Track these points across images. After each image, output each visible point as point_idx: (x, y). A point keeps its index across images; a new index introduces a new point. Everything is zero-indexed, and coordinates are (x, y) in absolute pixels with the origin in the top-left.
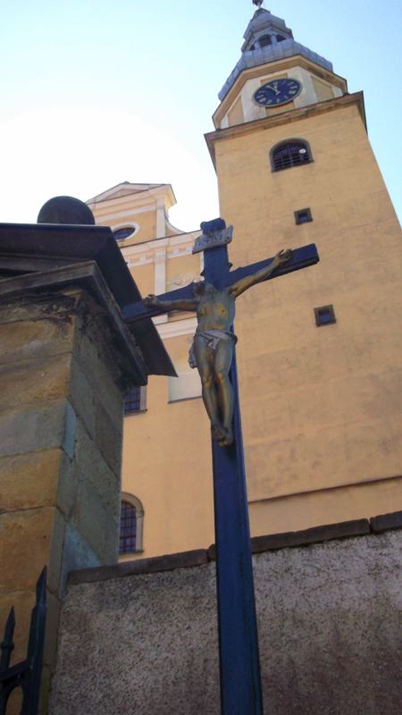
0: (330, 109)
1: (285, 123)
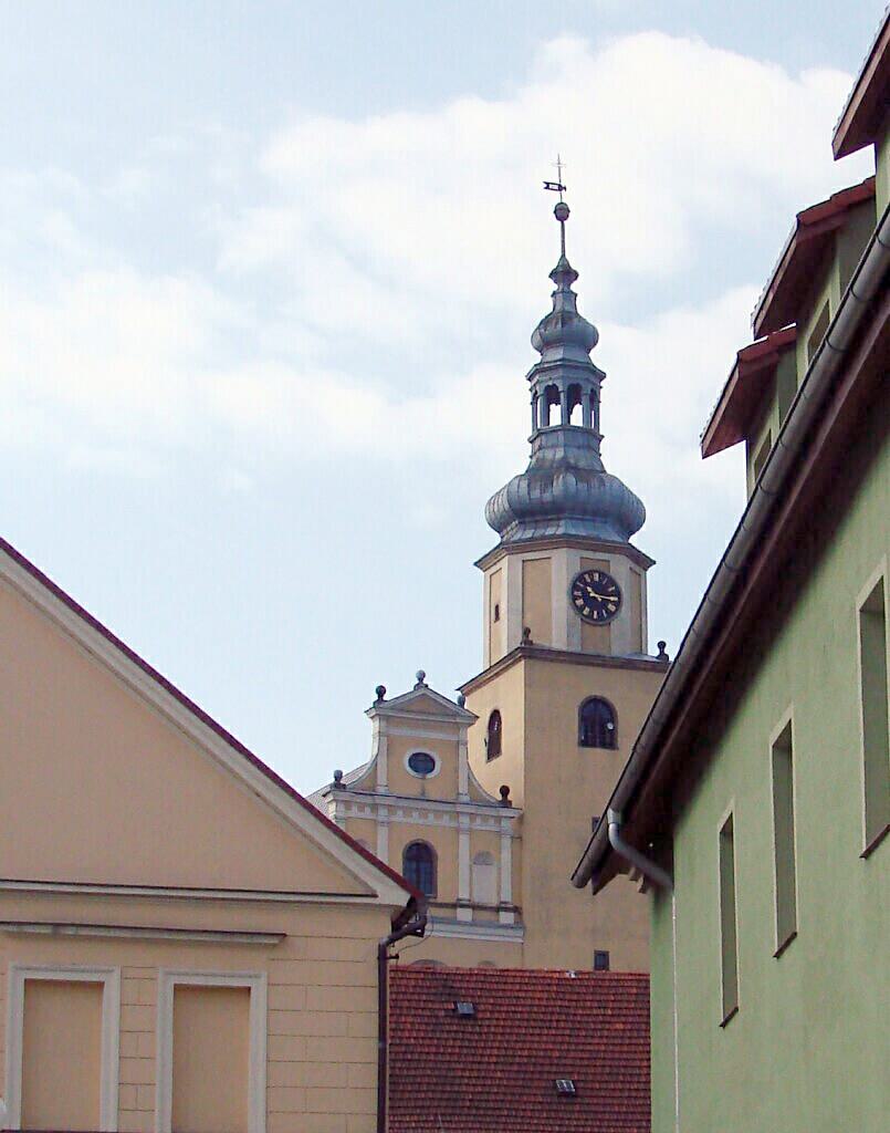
0: (645, 669)
1: (598, 665)
